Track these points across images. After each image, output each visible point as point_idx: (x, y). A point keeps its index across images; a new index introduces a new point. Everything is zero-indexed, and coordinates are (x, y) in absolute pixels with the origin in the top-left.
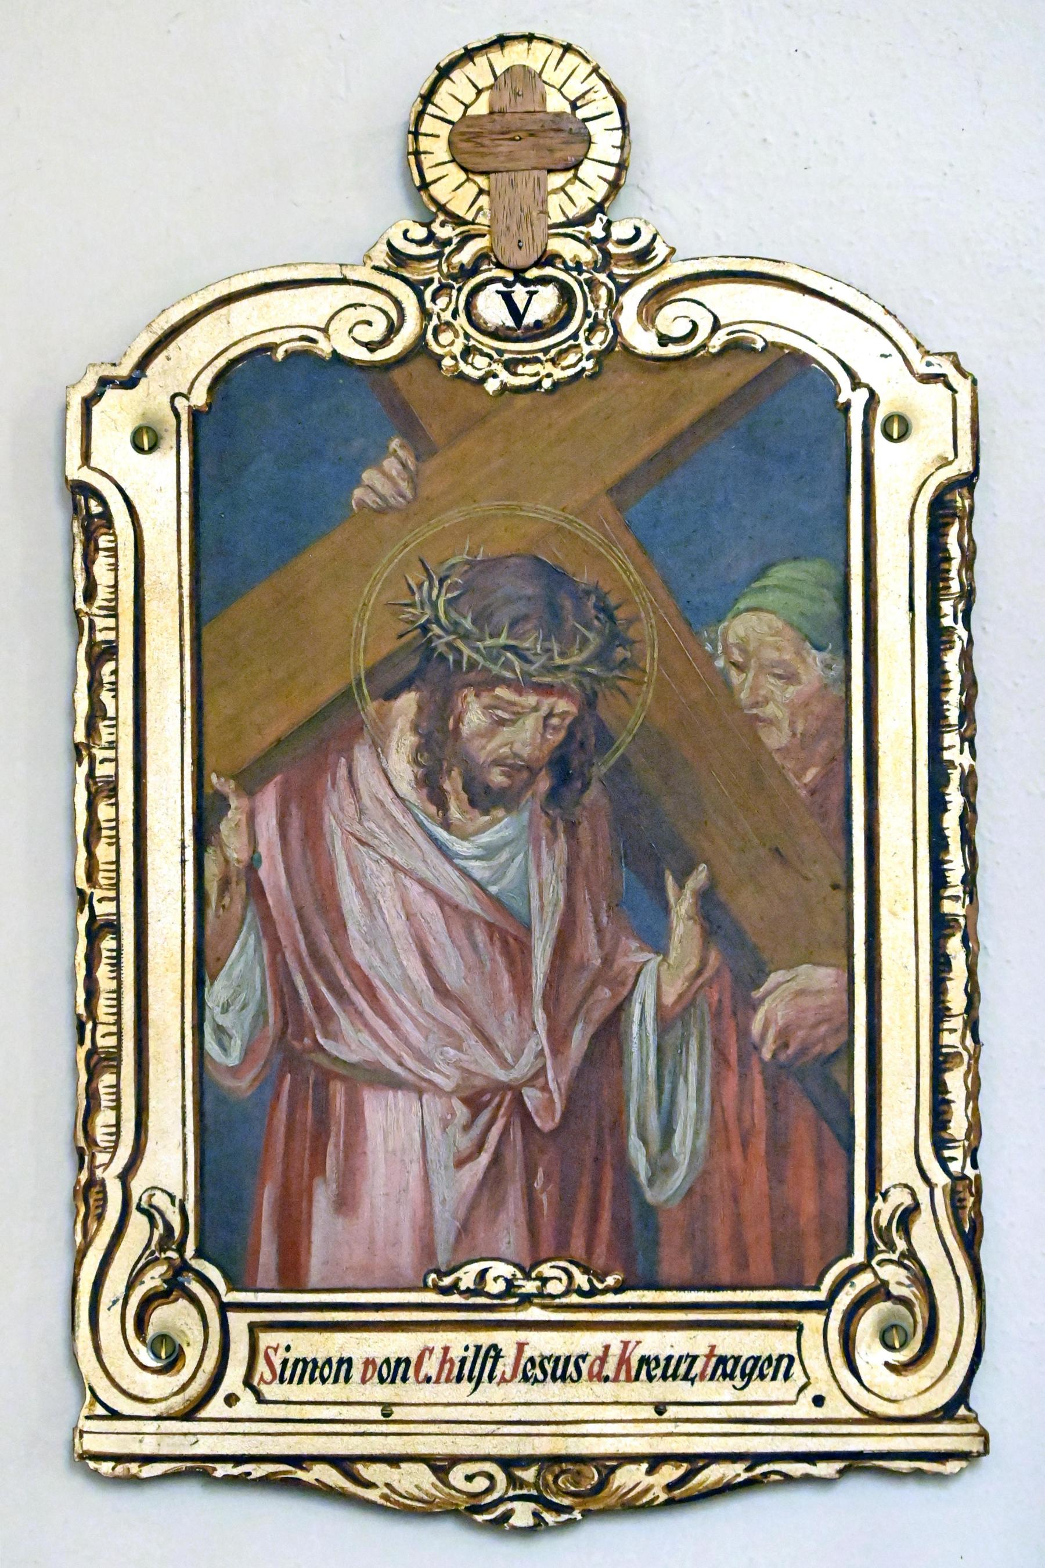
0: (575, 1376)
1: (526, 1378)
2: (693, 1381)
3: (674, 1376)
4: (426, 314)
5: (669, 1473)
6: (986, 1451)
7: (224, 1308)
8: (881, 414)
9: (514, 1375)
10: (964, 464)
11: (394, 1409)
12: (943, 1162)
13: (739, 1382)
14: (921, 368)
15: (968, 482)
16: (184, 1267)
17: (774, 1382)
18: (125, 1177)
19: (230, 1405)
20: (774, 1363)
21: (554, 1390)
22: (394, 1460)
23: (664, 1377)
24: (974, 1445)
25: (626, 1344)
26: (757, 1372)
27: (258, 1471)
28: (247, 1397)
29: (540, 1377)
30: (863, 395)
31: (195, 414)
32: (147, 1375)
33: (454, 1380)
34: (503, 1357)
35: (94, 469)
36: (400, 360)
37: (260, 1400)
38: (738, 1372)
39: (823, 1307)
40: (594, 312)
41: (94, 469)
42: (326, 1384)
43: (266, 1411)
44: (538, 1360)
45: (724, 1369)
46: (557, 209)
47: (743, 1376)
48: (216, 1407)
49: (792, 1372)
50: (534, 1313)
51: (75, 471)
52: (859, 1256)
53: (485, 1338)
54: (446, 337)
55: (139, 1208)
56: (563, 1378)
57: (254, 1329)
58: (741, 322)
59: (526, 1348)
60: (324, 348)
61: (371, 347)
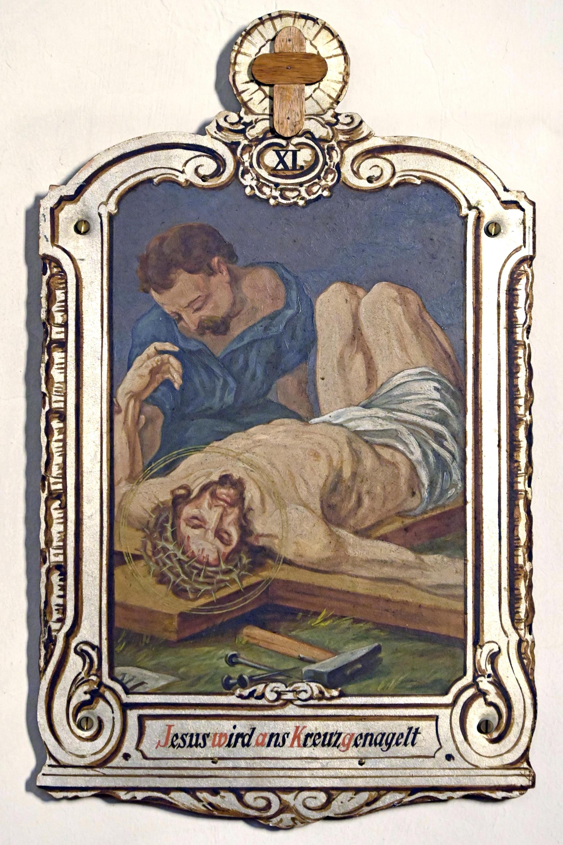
0: (281, 744)
1: (173, 745)
2: (338, 747)
3: (329, 744)
4: (238, 163)
5: (364, 796)
6: (533, 785)
7: (125, 707)
8: (485, 222)
9: (166, 743)
10: (527, 251)
11: (367, 760)
12: (516, 629)
13: (384, 747)
14: (505, 196)
15: (529, 260)
16: (101, 684)
17: (364, 748)
18: (70, 635)
19: (127, 760)
20: (364, 737)
21: (319, 752)
22: (215, 791)
23: (323, 745)
24: (524, 781)
25: (297, 728)
26: (352, 743)
27: (140, 795)
28: (136, 756)
29: (182, 745)
30: (472, 215)
31: (111, 217)
32: (86, 743)
33: (410, 744)
34: (420, 733)
35: (58, 247)
36: (221, 188)
37: (145, 757)
38: (384, 742)
39: (453, 704)
40: (329, 163)
41: (58, 247)
42: (359, 747)
43: (147, 763)
44: (180, 736)
45: (243, 742)
46: (310, 107)
47: (386, 744)
48: (118, 761)
49: (415, 742)
50: (290, 710)
51: (46, 248)
52: (468, 679)
53: (415, 724)
54: (248, 177)
55: (76, 652)
56: (197, 745)
57: (141, 719)
58: (440, 176)
59: (172, 728)
60: (181, 178)
61: (204, 178)
